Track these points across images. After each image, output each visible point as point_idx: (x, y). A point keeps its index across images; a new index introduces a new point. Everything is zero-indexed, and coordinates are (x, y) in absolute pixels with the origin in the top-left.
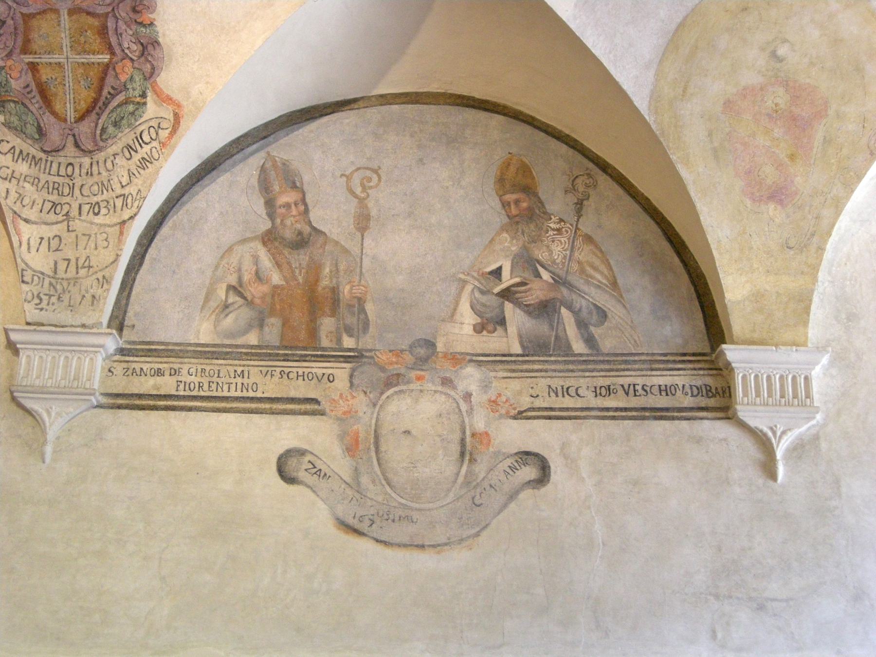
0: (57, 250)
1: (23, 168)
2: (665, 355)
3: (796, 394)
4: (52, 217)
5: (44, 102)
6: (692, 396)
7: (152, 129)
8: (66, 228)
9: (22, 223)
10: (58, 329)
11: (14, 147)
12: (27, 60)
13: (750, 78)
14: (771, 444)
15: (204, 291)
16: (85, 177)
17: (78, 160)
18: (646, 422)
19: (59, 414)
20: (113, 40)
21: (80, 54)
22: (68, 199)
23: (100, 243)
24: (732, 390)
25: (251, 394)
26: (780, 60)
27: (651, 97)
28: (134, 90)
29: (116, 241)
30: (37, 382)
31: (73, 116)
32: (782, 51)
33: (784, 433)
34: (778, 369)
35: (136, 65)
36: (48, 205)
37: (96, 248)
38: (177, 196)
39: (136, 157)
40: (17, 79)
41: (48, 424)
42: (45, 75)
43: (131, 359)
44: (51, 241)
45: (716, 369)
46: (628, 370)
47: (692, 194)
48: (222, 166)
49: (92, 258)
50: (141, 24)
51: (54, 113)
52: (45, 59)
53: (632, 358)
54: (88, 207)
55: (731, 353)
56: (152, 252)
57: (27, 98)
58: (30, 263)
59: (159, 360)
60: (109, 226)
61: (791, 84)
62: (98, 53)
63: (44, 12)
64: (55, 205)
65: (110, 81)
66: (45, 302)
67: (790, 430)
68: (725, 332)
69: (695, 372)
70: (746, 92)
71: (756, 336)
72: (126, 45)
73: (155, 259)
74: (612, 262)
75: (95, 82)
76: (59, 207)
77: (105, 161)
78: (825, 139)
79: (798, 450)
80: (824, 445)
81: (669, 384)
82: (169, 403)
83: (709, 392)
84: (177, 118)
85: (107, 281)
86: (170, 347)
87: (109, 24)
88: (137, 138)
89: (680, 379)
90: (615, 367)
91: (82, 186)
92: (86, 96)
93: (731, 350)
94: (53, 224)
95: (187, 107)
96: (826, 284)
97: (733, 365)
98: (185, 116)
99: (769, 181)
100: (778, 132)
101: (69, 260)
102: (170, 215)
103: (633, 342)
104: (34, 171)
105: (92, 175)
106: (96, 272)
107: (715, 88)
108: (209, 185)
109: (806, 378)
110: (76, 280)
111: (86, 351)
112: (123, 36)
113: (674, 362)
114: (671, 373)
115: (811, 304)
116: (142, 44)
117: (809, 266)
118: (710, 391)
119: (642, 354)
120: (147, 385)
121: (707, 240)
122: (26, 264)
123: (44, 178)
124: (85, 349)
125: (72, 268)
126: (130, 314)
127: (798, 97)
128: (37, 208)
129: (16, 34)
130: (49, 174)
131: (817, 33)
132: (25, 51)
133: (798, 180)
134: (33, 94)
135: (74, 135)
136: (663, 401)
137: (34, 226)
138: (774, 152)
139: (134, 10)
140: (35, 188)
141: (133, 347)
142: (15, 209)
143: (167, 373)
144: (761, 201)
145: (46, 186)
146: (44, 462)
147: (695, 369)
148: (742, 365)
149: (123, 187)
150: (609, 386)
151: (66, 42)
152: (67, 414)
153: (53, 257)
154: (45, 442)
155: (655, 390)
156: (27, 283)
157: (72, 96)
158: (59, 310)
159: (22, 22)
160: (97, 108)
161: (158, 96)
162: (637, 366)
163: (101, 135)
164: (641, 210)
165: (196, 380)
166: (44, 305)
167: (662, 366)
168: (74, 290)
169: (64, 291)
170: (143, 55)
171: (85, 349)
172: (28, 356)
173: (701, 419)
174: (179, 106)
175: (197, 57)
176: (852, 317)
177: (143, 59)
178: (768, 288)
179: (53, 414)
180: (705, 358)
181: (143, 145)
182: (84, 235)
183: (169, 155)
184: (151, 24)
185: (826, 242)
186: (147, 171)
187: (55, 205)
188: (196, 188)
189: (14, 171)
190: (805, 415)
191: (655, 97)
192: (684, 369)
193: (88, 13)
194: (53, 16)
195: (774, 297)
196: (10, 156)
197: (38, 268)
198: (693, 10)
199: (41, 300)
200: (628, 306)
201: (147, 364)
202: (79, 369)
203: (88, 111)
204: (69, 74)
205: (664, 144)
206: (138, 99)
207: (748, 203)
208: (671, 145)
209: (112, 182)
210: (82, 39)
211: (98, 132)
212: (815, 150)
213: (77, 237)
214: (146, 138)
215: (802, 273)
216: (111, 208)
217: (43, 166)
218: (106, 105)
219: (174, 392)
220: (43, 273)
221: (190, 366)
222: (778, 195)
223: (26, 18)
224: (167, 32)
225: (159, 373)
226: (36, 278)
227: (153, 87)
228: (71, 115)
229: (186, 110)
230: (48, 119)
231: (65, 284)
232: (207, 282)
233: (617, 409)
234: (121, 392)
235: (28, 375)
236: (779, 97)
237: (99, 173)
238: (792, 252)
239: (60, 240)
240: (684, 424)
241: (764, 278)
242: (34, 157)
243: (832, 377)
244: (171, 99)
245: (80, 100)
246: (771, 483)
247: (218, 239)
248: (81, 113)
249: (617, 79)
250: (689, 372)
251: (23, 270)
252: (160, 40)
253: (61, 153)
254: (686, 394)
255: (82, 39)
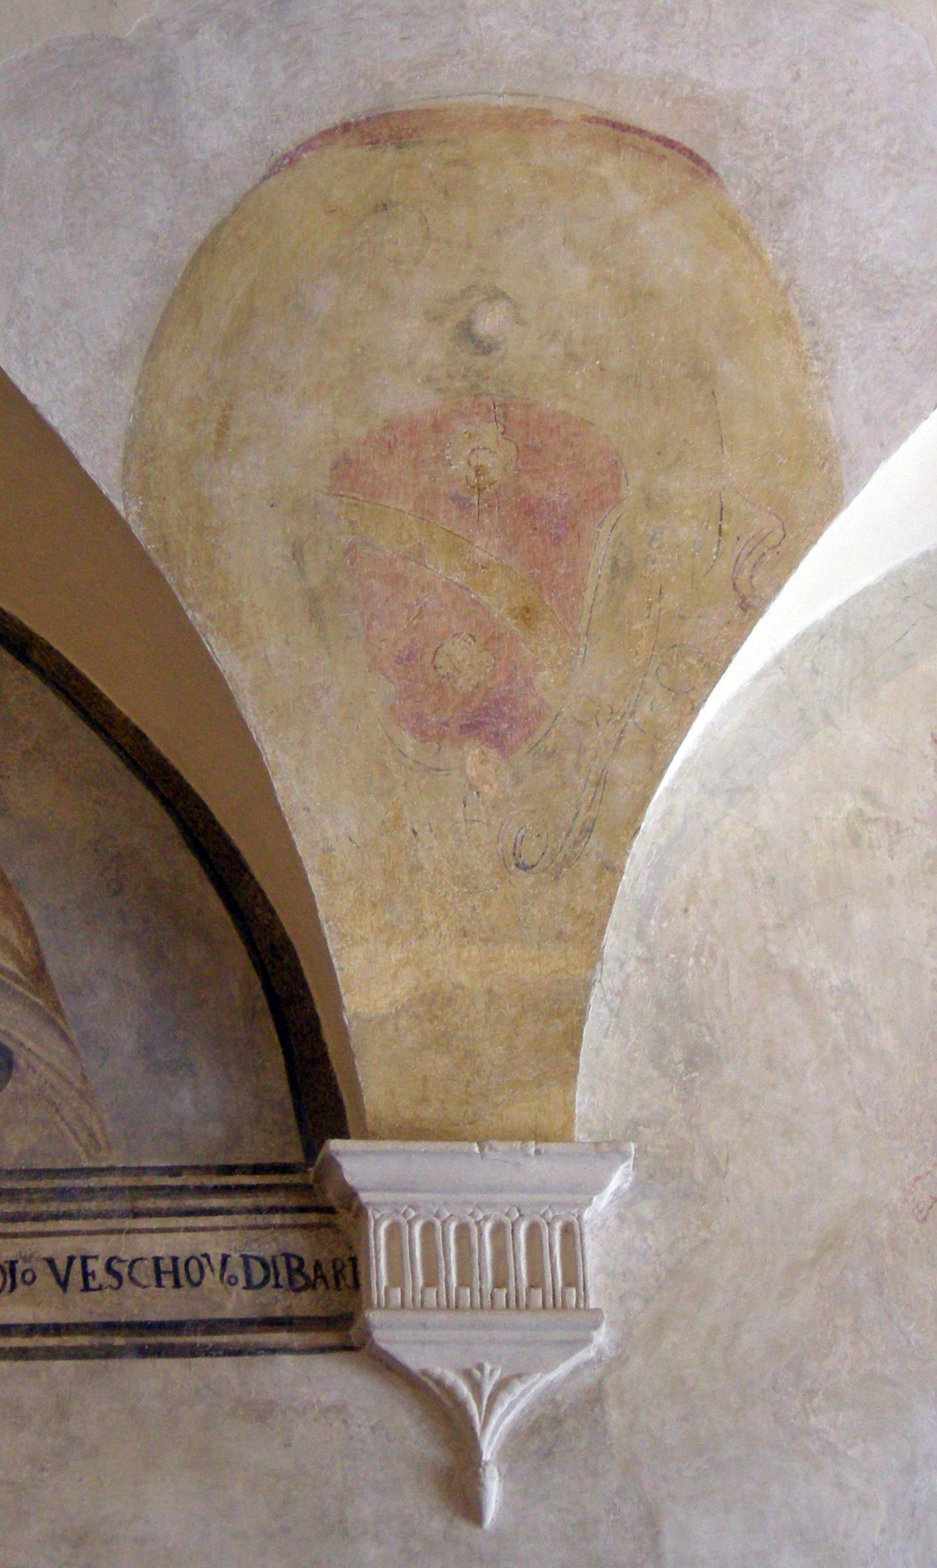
2: (174, 1171)
3: (541, 1278)
6: (249, 1286)
13: (403, 397)
14: (469, 1420)
18: (114, 1363)
24: (361, 1268)
26: (485, 348)
27: (129, 448)
32: (489, 323)
33: (503, 1385)
34: (494, 1205)
45: (318, 1209)
46: (68, 1216)
47: (251, 719)
53: (80, 1183)
55: (356, 1162)
61: (517, 413)
67: (519, 1376)
68: (346, 1102)
69: (260, 1219)
70: (396, 437)
71: (429, 1113)
74: (33, 913)
78: (615, 564)
79: (542, 1435)
80: (615, 1418)
81: (183, 1256)
83: (295, 1273)
89: (214, 1239)
90: (32, 1209)
93: (354, 1154)
96: (631, 966)
97: (364, 1197)
99: (464, 684)
100: (485, 547)
103: (83, 1136)
107: (307, 425)
109: (567, 1230)
113: (201, 1190)
114: (191, 1222)
115: (582, 1022)
117: (579, 917)
118: (299, 1270)
119: (110, 1170)
121: (292, 845)
127: (538, 451)
131: (581, 274)
133: (545, 677)
136: (164, 1304)
138: (476, 603)
144: (441, 737)
147: (258, 1210)
148: (390, 1197)
150: (13, 1263)
155: (144, 1272)
162: (93, 1206)
164: (120, 765)
167: (163, 1203)
173: (273, 1351)
176: (700, 1057)
178: (464, 979)
180: (286, 1179)
185: (623, 849)
190: (562, 1335)
191: (140, 449)
192: (229, 1212)
195: (480, 1005)
198: (237, 208)
200: (73, 1034)
205: (169, 579)
207: (409, 742)
208: (188, 581)
212: (588, 596)
215: (560, 935)
222: (489, 719)
233: (31, 1330)
236: (484, 450)
238: (530, 879)
240: (224, 1366)
241: (453, 950)
243: (642, 1224)
246: (464, 1528)
249: (31, 398)
250: (241, 1219)
254: (233, 1280)
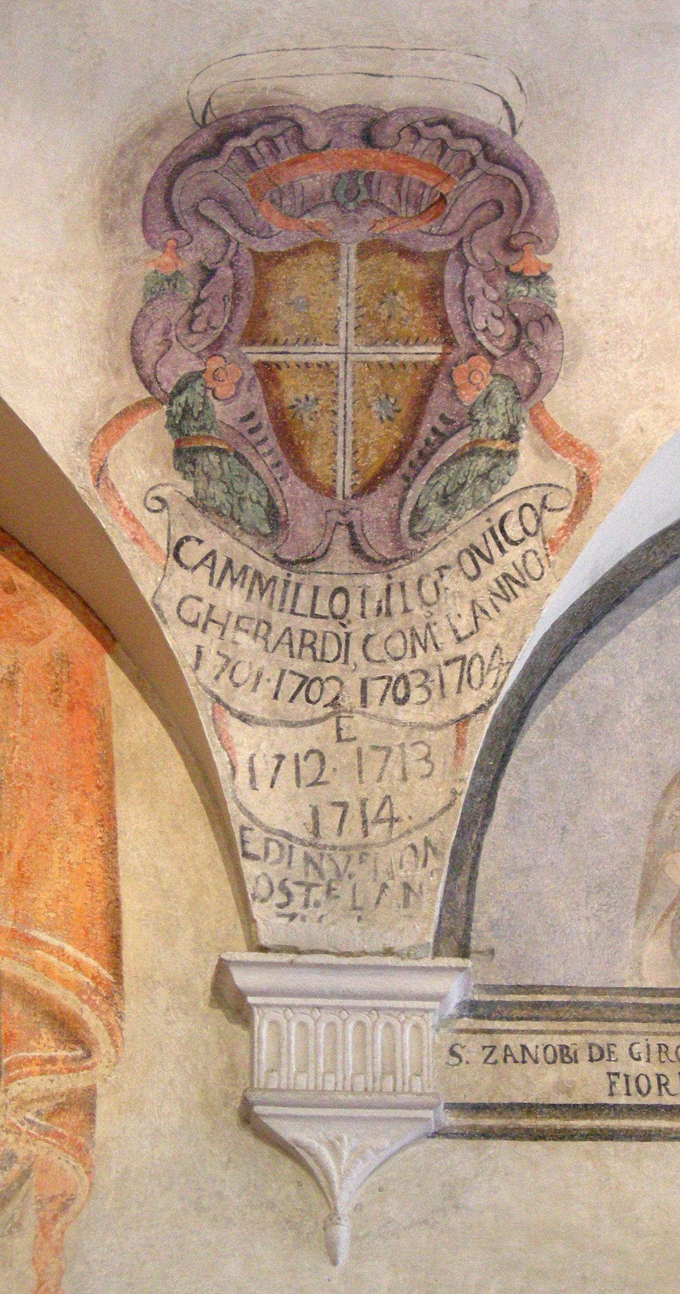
0: (316, 783)
1: (232, 599)
4: (301, 710)
5: (286, 452)
7: (527, 510)
8: (334, 733)
9: (235, 723)
10: (345, 961)
11: (213, 553)
12: (254, 358)
15: (638, 871)
16: (373, 619)
17: (358, 580)
19: (359, 1153)
20: (453, 312)
21: (373, 344)
22: (335, 669)
23: (411, 765)
25: (652, 1099)
28: (491, 423)
29: (450, 760)
30: (302, 1081)
31: (348, 484)
35: (500, 368)
36: (291, 684)
37: (405, 779)
38: (547, 661)
39: (491, 574)
40: (227, 401)
41: (335, 1177)
42: (293, 389)
43: (497, 1025)
44: (302, 763)
48: (637, 594)
49: (397, 800)
50: (519, 276)
51: (307, 477)
52: (298, 355)
54: (382, 684)
56: (508, 786)
57: (247, 442)
58: (263, 815)
59: (561, 1026)
60: (432, 728)
62: (417, 341)
63: (305, 249)
64: (306, 682)
65: (438, 403)
66: (298, 900)
72: (480, 325)
73: (518, 801)
75: (404, 406)
76: (316, 687)
77: (420, 582)
82: (598, 1123)
84: (585, 484)
85: (434, 850)
86: (581, 998)
87: (447, 277)
88: (492, 530)
91: (368, 638)
92: (381, 437)
94: (304, 724)
95: (609, 460)
98: (604, 482)
101: (344, 805)
102: (538, 701)
104: (258, 607)
105: (389, 613)
106: (409, 832)
108: (613, 635)
110: (363, 851)
111: (403, 1010)
112: (477, 304)
116: (517, 322)
120: (542, 1083)
122: (249, 815)
123: (280, 621)
124: (400, 1004)
125: (353, 824)
126: (480, 923)
128: (266, 688)
129: (236, 301)
130: (292, 612)
132: (252, 337)
134: (263, 433)
135: (350, 526)
137: (262, 730)
139: (508, 247)
140: (260, 643)
141: (496, 998)
142: (217, 691)
143: (583, 1055)
145: (286, 639)
146: (334, 1263)
149: (459, 639)
151: (347, 316)
152: (377, 1152)
153: (306, 799)
154: (333, 1217)
156: (255, 858)
157: (350, 438)
158: (330, 918)
159: (251, 273)
160: (405, 465)
161: (545, 438)
163: (412, 525)
165: (652, 1069)
166: (296, 905)
168: (362, 873)
169: (339, 875)
170: (516, 344)
171: (400, 1004)
172: (274, 1023)
174: (591, 458)
175: (638, 350)
177: (516, 353)
179: (346, 1153)
181: (506, 546)
182: (376, 748)
183: (566, 568)
184: (542, 277)
186: (514, 603)
187: (306, 682)
188: (587, 643)
189: (212, 607)
193: (403, 253)
194: (324, 259)
196: (203, 573)
197: (277, 824)
199: (289, 895)
201: (537, 1037)
202: (392, 1048)
203: (386, 472)
204: (346, 388)
206: (499, 444)
209: (434, 629)
210: (384, 311)
211: (405, 518)
213: (359, 753)
214: (513, 530)
216: (435, 686)
217: (278, 596)
218: (424, 457)
219: (604, 1099)
220: (288, 836)
221: (633, 1038)
223: (263, 264)
224: (576, 296)
225: (565, 1055)
226: (273, 846)
227: (534, 417)
228: (345, 480)
229: (605, 467)
230: (293, 490)
231: (340, 858)
232: (642, 849)
234: (485, 1100)
235: (280, 1064)
237: (406, 610)
239: (323, 761)
242: (258, 575)
244: (573, 444)
245: (366, 446)
247: (650, 754)
248: (369, 475)
251: (243, 829)
252: (558, 312)
253: (320, 566)
255: (384, 311)
